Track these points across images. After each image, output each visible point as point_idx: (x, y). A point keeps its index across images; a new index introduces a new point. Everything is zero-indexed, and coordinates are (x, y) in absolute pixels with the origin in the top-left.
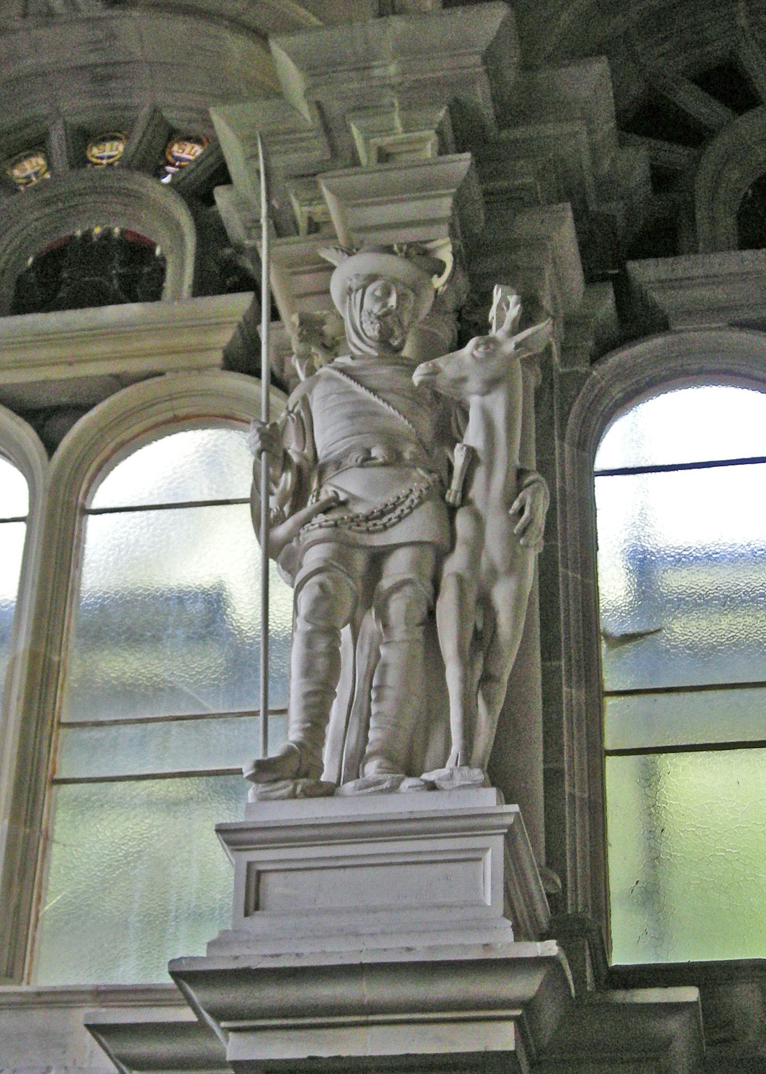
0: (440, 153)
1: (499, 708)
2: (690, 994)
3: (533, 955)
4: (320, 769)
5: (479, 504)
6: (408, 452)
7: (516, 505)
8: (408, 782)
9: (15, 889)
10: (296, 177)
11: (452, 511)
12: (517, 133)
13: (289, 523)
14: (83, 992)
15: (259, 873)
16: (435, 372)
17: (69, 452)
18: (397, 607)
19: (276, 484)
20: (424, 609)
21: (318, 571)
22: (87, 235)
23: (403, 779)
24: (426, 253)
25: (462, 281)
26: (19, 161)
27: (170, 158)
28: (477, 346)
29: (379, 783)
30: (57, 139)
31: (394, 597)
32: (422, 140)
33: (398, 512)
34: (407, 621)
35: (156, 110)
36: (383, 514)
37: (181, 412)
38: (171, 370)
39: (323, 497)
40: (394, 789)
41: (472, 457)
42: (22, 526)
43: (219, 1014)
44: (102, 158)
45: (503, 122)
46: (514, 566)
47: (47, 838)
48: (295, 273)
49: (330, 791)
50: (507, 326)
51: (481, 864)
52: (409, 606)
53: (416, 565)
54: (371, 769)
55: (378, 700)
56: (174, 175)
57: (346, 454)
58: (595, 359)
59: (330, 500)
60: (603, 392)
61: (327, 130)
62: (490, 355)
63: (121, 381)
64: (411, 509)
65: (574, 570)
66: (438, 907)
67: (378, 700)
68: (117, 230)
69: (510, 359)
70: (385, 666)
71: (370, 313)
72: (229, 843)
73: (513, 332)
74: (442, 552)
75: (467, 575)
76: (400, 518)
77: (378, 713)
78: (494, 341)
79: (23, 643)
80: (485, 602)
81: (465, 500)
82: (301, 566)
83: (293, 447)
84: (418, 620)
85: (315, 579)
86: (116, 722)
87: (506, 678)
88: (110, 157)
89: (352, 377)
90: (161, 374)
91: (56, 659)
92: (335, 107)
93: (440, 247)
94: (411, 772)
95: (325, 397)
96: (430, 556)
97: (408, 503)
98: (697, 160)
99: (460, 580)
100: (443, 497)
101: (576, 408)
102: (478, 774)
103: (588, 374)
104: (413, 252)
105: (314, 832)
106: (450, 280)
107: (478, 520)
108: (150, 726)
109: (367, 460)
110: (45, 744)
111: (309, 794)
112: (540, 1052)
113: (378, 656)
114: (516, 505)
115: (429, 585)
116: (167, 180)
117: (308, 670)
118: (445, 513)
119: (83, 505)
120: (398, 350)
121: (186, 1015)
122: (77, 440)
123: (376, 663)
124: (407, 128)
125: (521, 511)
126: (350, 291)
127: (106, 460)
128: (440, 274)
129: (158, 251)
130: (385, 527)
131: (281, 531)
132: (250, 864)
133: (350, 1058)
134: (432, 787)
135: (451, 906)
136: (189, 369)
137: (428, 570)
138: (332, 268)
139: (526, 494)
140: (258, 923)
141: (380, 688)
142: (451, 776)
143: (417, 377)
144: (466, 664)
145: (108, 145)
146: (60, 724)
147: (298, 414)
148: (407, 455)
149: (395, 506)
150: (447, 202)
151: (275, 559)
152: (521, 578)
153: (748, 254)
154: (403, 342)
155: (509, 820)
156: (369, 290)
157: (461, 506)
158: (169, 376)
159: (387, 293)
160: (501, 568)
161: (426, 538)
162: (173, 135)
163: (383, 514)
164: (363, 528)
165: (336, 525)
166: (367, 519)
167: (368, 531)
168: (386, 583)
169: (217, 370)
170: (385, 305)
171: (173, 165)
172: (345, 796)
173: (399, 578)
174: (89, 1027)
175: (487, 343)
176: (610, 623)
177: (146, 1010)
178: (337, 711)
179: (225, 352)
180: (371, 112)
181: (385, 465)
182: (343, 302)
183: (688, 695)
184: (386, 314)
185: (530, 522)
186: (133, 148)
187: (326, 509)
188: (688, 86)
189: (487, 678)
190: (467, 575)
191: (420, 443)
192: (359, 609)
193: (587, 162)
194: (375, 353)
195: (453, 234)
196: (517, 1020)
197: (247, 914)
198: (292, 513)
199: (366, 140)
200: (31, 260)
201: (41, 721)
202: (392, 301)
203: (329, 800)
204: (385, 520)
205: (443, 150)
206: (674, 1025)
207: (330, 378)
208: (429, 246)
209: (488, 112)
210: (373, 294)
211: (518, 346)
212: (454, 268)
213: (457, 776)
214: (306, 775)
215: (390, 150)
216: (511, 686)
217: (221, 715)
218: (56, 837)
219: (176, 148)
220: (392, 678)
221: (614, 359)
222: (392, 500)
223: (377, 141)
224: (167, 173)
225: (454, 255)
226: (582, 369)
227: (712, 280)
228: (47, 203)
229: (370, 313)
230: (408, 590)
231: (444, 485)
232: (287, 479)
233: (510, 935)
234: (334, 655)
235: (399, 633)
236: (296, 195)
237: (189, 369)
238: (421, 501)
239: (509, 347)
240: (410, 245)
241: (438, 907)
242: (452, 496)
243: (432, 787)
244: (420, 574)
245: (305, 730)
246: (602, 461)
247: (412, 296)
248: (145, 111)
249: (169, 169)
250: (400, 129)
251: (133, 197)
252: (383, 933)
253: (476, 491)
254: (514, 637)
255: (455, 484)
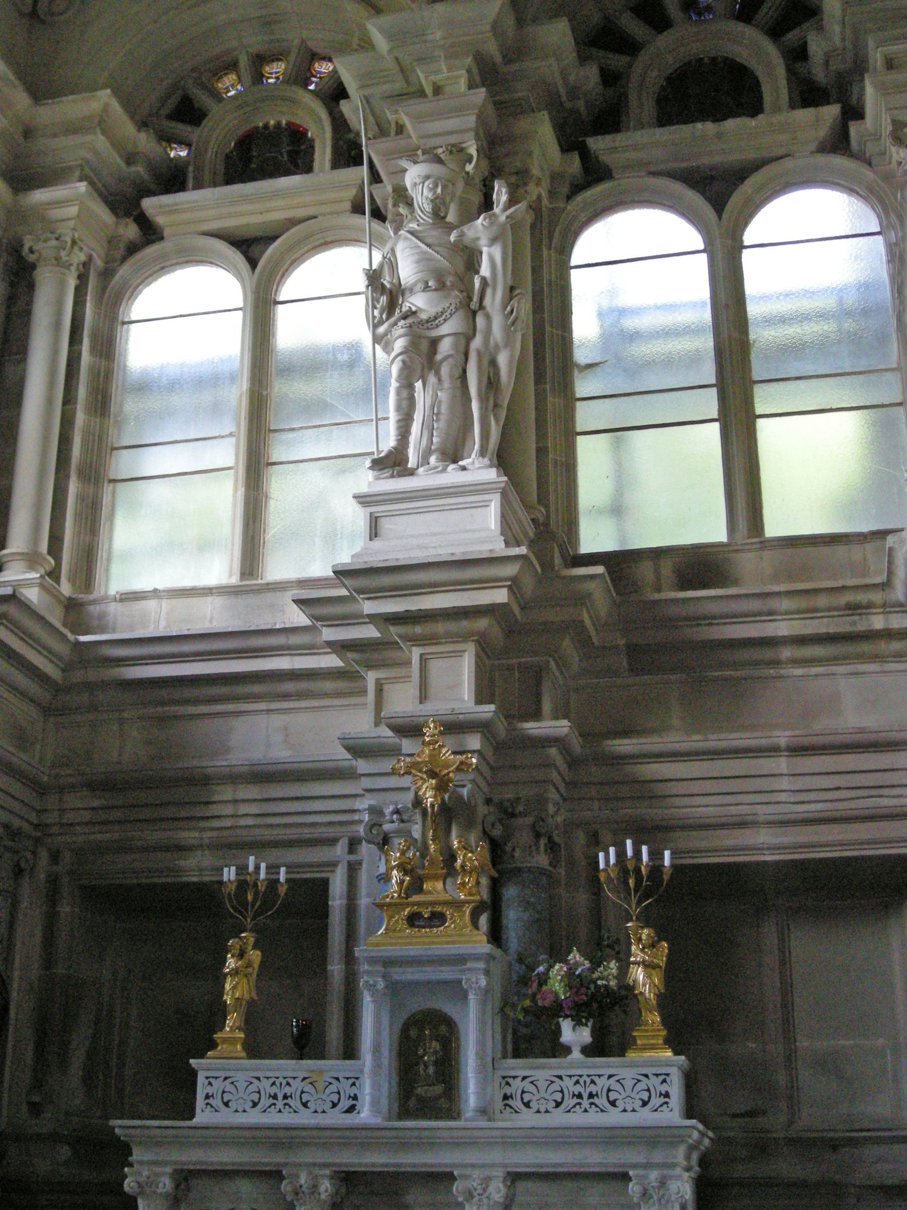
0: (469, 89)
1: (501, 424)
2: (600, 569)
3: (514, 554)
4: (407, 461)
5: (489, 308)
6: (449, 281)
7: (509, 308)
8: (452, 467)
9: (251, 527)
10: (388, 97)
11: (474, 313)
12: (515, 67)
13: (386, 325)
14: (291, 582)
15: (376, 518)
16: (462, 235)
17: (264, 268)
18: (445, 370)
19: (378, 302)
20: (461, 370)
21: (401, 354)
22: (266, 126)
23: (448, 466)
24: (461, 150)
25: (485, 164)
26: (221, 77)
27: (314, 73)
28: (485, 219)
29: (436, 468)
30: (243, 61)
31: (444, 364)
32: (458, 77)
33: (444, 317)
34: (451, 377)
35: (303, 41)
36: (436, 318)
37: (328, 239)
38: (321, 215)
39: (404, 309)
40: (444, 470)
41: (484, 281)
42: (240, 313)
43: (360, 591)
44: (271, 73)
45: (508, 61)
46: (508, 342)
47: (266, 497)
48: (388, 160)
49: (412, 473)
50: (501, 206)
51: (488, 508)
52: (451, 369)
53: (455, 345)
54: (433, 460)
55: (438, 420)
56: (317, 84)
57: (415, 284)
58: (569, 198)
59: (407, 311)
60: (575, 217)
61: (402, 71)
62: (491, 224)
63: (293, 222)
64: (451, 315)
65: (557, 330)
66: (467, 531)
67: (438, 420)
68: (284, 122)
69: (504, 224)
70: (440, 402)
71: (427, 198)
72: (360, 503)
73: (505, 209)
74: (469, 337)
75: (483, 350)
76: (445, 320)
77: (438, 428)
78: (494, 215)
79: (245, 385)
80: (493, 363)
81: (481, 307)
82: (393, 349)
83: (387, 281)
84: (457, 376)
85: (400, 358)
86: (302, 428)
87: (505, 405)
88: (276, 73)
89: (418, 238)
90: (315, 217)
91: (265, 393)
92: (406, 60)
93: (470, 146)
94: (455, 461)
95: (403, 250)
96: (463, 341)
97: (449, 311)
98: (630, 66)
99: (479, 353)
100: (469, 306)
101: (557, 230)
102: (486, 461)
103: (565, 208)
104: (454, 150)
105: (404, 495)
106: (476, 167)
107: (488, 317)
108: (321, 429)
109: (426, 288)
110: (262, 444)
111: (401, 475)
112: (525, 603)
113: (437, 395)
114: (509, 308)
115: (463, 357)
116: (312, 87)
117: (398, 408)
118: (470, 315)
119: (275, 300)
120: (444, 217)
121: (344, 592)
122: (268, 261)
123: (435, 402)
124: (450, 69)
125: (512, 312)
126: (415, 185)
127: (287, 270)
128: (470, 162)
129: (309, 135)
130: (437, 326)
131: (381, 330)
132: (371, 514)
133: (426, 610)
134: (464, 468)
135: (474, 531)
136: (331, 213)
137: (462, 349)
138: (406, 170)
139: (514, 302)
140: (377, 544)
141: (438, 414)
142: (473, 463)
143: (452, 238)
144: (483, 400)
145: (275, 64)
146: (270, 430)
147: (389, 259)
148: (448, 283)
149: (442, 313)
150: (474, 118)
151: (379, 344)
152: (512, 349)
153: (659, 131)
154: (447, 214)
155: (503, 485)
156: (426, 184)
157: (479, 309)
158: (320, 218)
159: (436, 186)
160: (501, 344)
161: (460, 331)
162: (314, 57)
163: (436, 318)
164: (425, 327)
165: (410, 326)
166: (427, 321)
167: (428, 328)
168: (439, 357)
169: (348, 213)
170: (435, 193)
171: (315, 77)
172: (418, 475)
173: (445, 354)
174: (294, 601)
175: (490, 217)
176: (581, 356)
177: (323, 590)
178: (415, 428)
179: (352, 202)
180: (428, 60)
181: (436, 290)
182: (412, 190)
183: (623, 399)
184: (436, 199)
185: (516, 319)
186: (291, 64)
187: (405, 317)
188: (628, 14)
189: (496, 406)
190: (483, 350)
191: (456, 274)
192: (426, 370)
193: (560, 82)
194: (431, 221)
195: (477, 138)
196: (509, 587)
197: (371, 539)
198: (387, 319)
199: (427, 80)
200: (233, 144)
201: (259, 429)
202: (439, 190)
203: (411, 477)
204: (437, 321)
205: (471, 86)
206: (591, 586)
207: (406, 238)
208: (464, 145)
209: (498, 59)
210: (428, 186)
211: (507, 217)
212: (478, 156)
213: (476, 462)
214: (399, 465)
215: (440, 83)
216: (509, 409)
217: (361, 421)
218: (272, 496)
219: (316, 65)
220: (444, 408)
221: (580, 198)
222: (441, 310)
223: (433, 78)
224: (312, 82)
225: (477, 151)
226: (562, 205)
227: (635, 147)
228: (240, 107)
229: (427, 198)
230: (450, 360)
231: (470, 299)
232: (384, 299)
233: (503, 545)
234: (411, 400)
235: (446, 384)
236: (388, 109)
237: (331, 213)
238: (456, 309)
239: (503, 218)
240: (453, 145)
241: (467, 531)
242: (474, 305)
243: (464, 468)
244: (457, 351)
245: (398, 440)
246: (574, 261)
247: (451, 186)
248: (296, 42)
249: (314, 79)
250: (445, 71)
251: (293, 101)
252: (440, 546)
253: (487, 301)
254: (509, 383)
255: (476, 298)
